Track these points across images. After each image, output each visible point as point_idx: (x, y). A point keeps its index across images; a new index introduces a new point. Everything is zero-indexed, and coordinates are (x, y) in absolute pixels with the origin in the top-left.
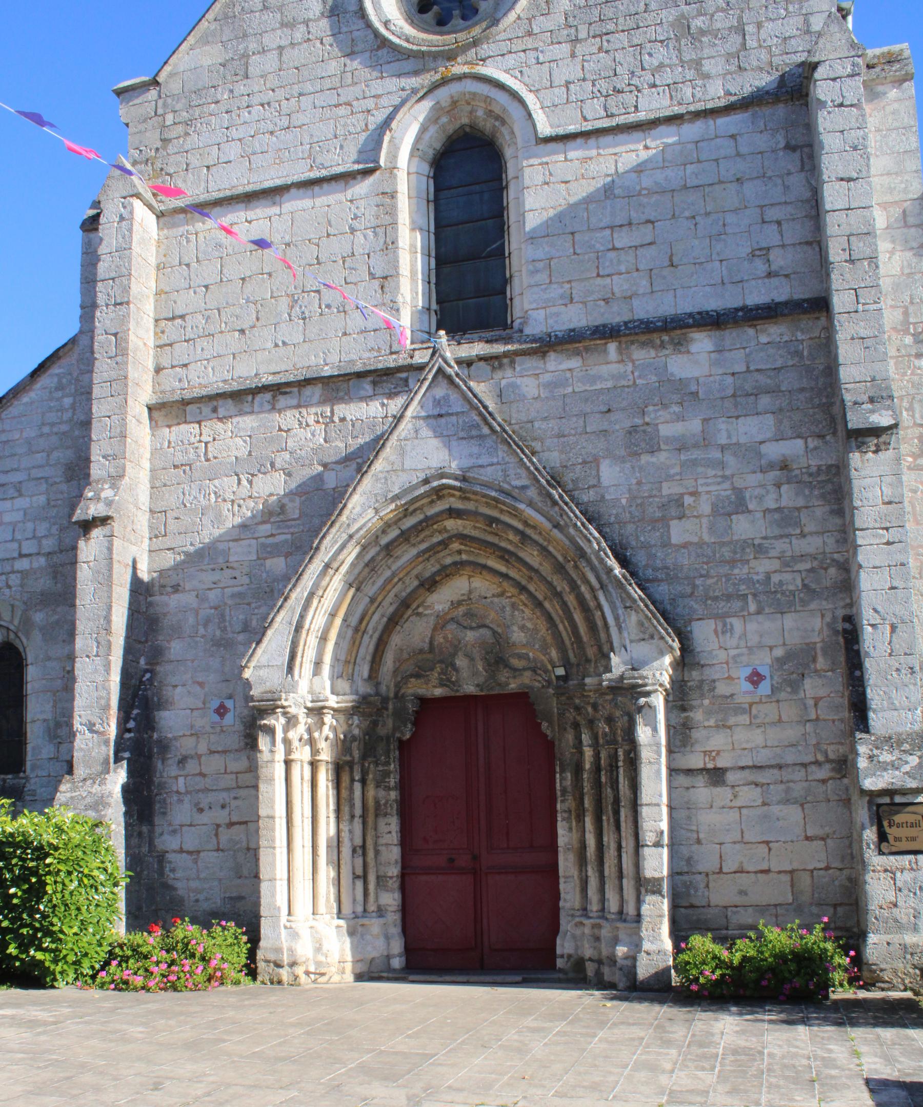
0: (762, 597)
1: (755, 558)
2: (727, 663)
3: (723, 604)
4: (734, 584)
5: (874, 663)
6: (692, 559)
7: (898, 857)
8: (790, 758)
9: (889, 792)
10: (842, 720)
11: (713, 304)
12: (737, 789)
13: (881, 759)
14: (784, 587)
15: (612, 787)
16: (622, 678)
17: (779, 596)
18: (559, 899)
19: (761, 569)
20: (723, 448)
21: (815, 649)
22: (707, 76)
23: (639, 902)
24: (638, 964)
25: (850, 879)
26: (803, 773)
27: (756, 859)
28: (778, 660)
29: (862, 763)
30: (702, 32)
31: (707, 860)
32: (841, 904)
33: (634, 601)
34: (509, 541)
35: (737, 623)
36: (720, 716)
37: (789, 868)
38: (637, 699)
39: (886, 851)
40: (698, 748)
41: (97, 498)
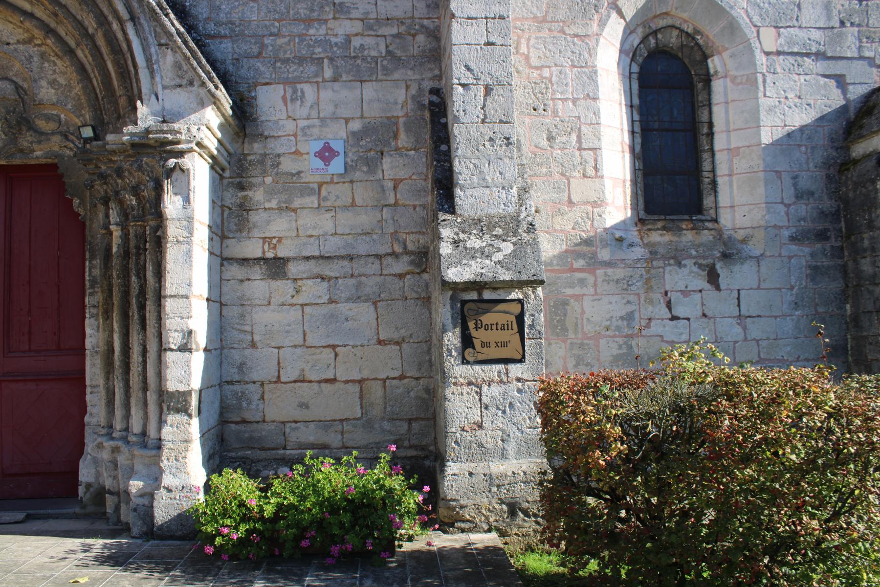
0: (340, 62)
1: (334, 18)
2: (295, 135)
3: (294, 67)
4: (309, 46)
5: (463, 130)
6: (262, 14)
7: (485, 367)
8: (362, 248)
9: (477, 285)
10: (424, 207)
12: (300, 283)
13: (469, 245)
14: (366, 53)
15: (138, 276)
16: (147, 131)
17: (359, 62)
18: (86, 412)
19: (341, 31)
21: (396, 124)
23: (161, 422)
24: (155, 504)
25: (427, 390)
26: (377, 266)
27: (320, 365)
28: (354, 134)
29: (445, 249)
31: (262, 366)
32: (416, 419)
33: (169, 35)
35: (309, 90)
36: (284, 197)
37: (357, 377)
38: (166, 160)
39: (471, 359)
40: (256, 233)
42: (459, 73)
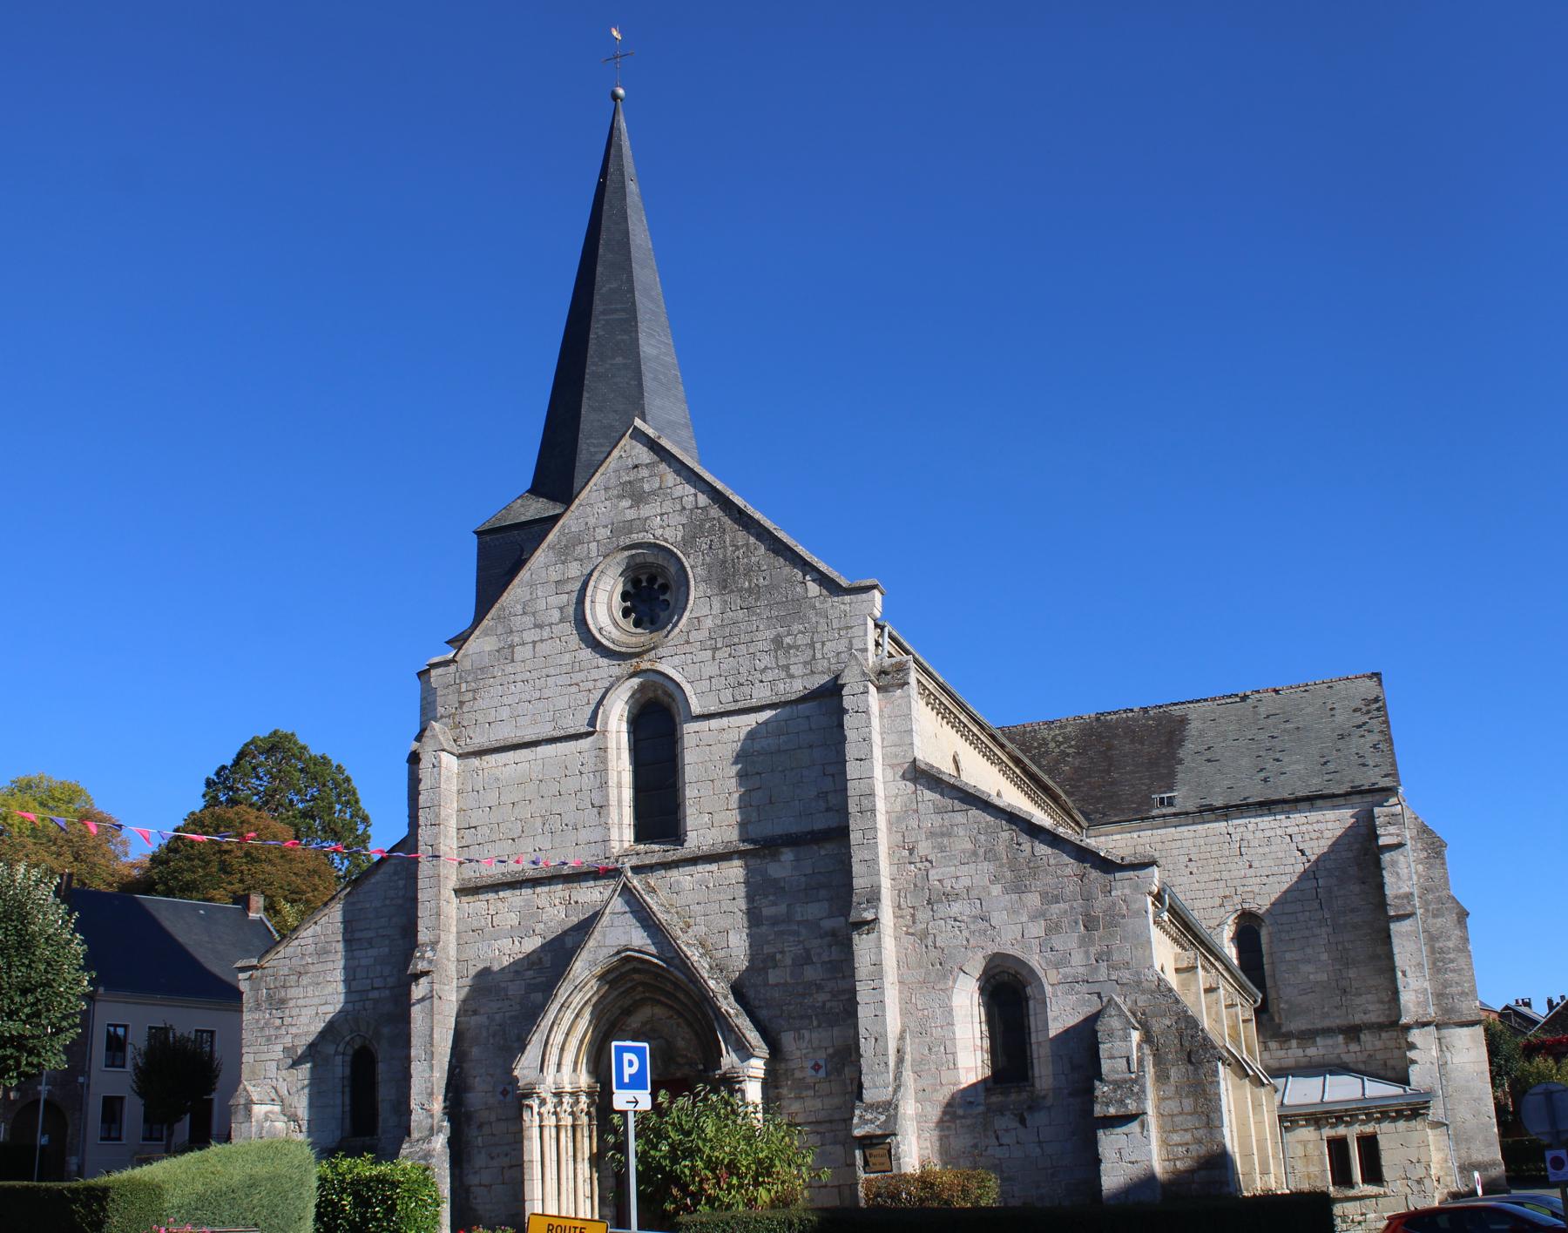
8: (836, 1117)
11: (795, 829)
20: (799, 923)
22: (792, 677)
29: (856, 1120)
30: (790, 647)
34: (669, 988)
35: (806, 1033)
41: (422, 958)
42: (862, 1031)
